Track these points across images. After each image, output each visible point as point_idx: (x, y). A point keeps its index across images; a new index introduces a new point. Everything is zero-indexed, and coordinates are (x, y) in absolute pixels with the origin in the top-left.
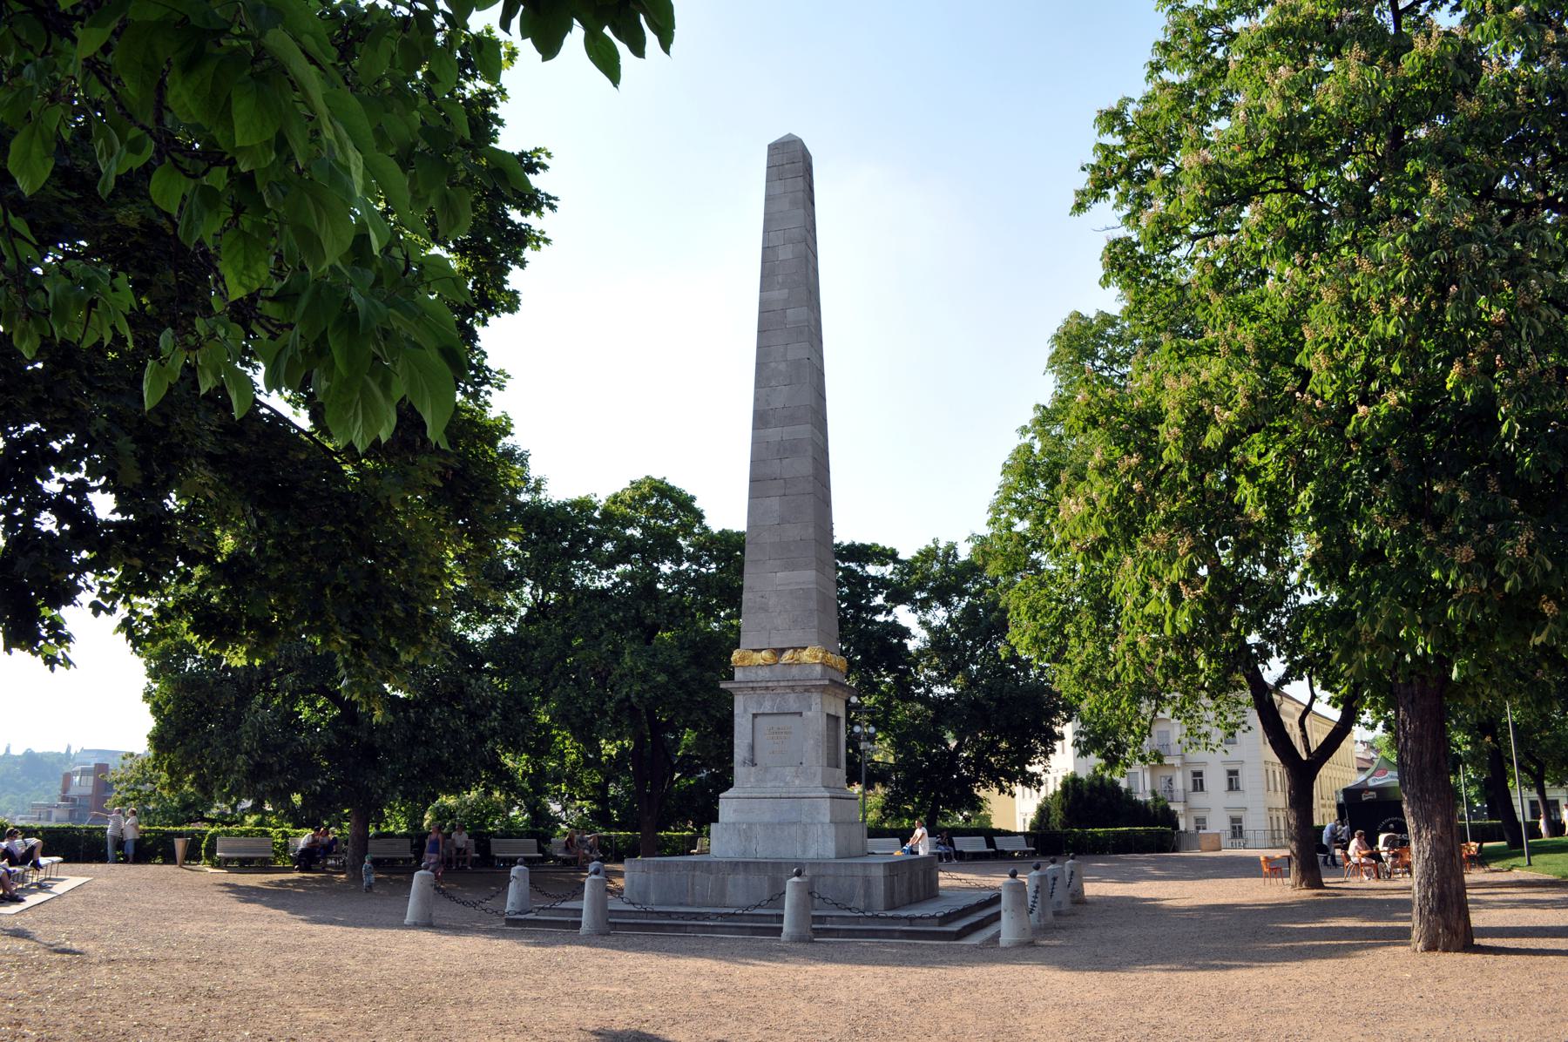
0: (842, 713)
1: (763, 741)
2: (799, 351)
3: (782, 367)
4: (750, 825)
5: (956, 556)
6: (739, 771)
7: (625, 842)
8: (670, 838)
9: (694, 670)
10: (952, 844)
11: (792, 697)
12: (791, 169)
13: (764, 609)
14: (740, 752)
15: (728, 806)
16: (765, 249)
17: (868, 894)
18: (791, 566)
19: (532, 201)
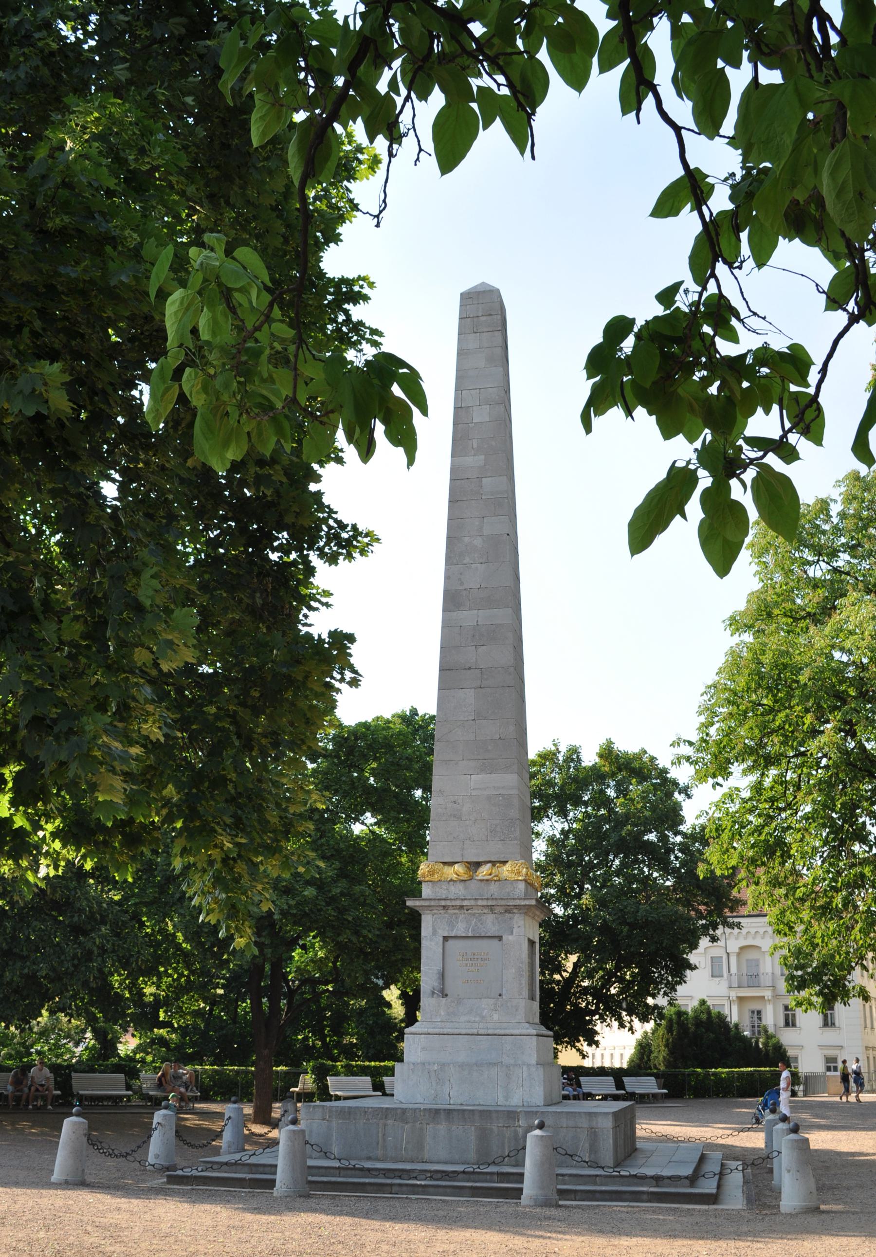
3: (478, 542)
4: (443, 1065)
5: (579, 760)
7: (211, 1077)
8: (212, 1065)
9: (343, 884)
10: (579, 1085)
11: (490, 918)
12: (639, 122)
13: (457, 816)
17: (594, 1148)
18: (488, 768)
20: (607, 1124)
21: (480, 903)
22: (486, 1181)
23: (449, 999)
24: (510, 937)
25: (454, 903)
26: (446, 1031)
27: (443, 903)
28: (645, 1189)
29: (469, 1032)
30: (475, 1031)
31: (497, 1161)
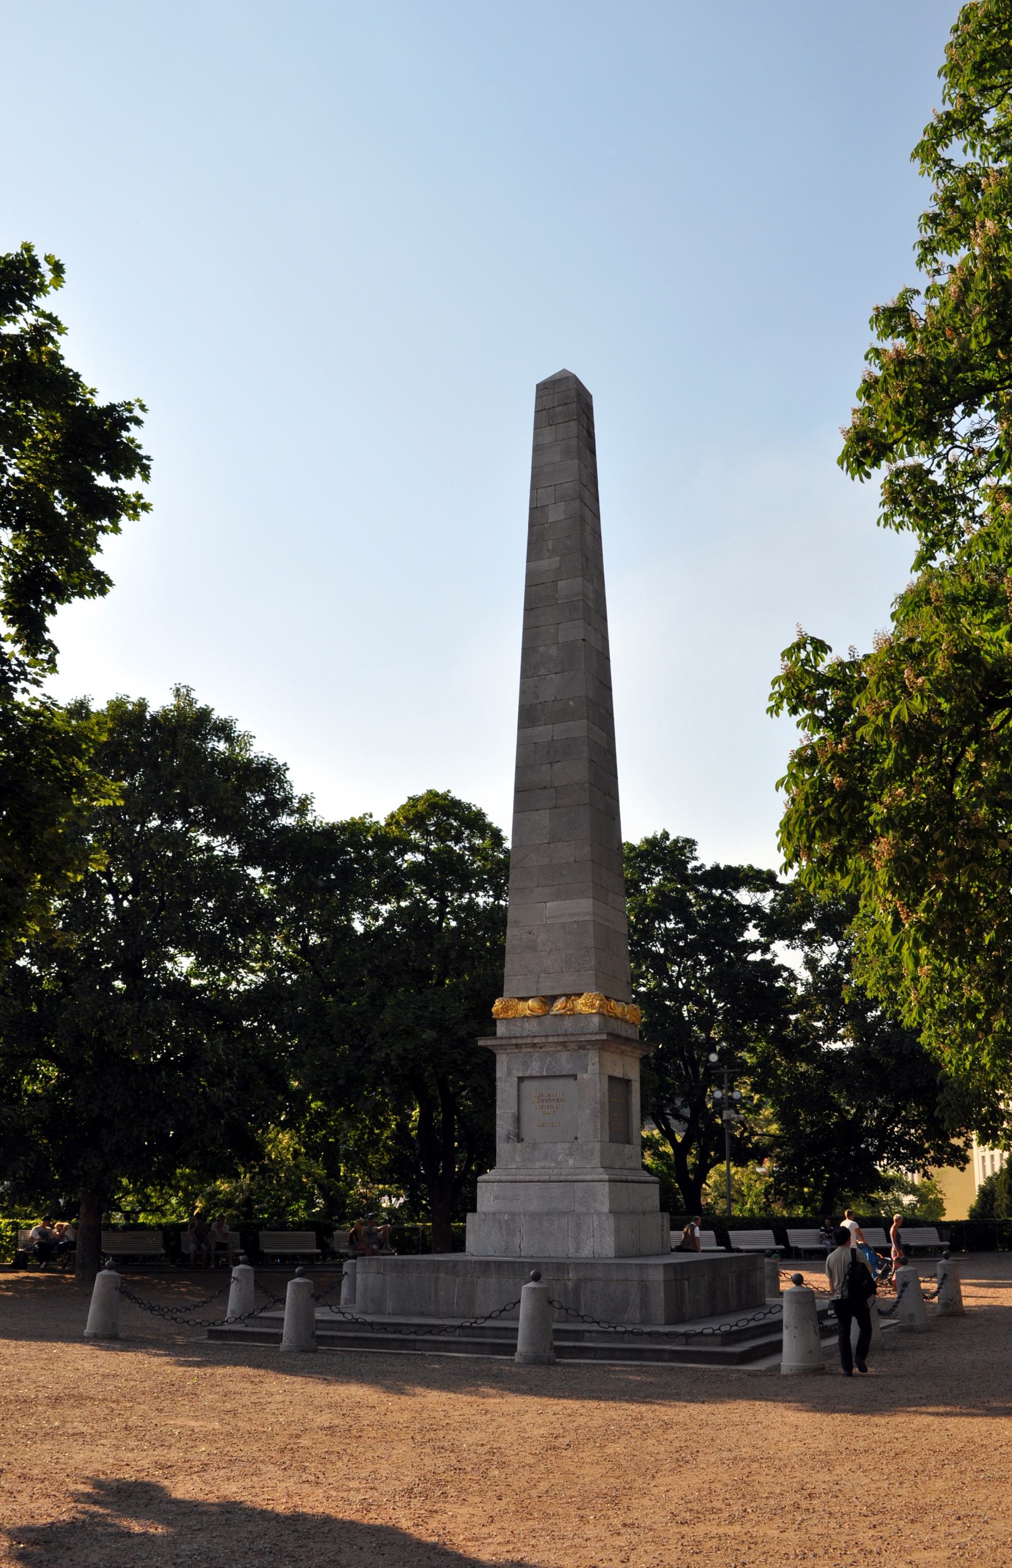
0: (634, 1074)
1: (531, 1112)
2: (574, 631)
3: (553, 651)
4: (513, 1215)
6: (502, 1148)
11: (564, 1056)
12: (565, 413)
13: (533, 948)
14: (503, 1125)
15: (489, 1193)
16: (533, 510)
19: (129, 461)
20: (657, 1276)
21: (551, 1039)
22: (326, 1330)
23: (525, 1144)
24: (585, 1076)
25: (524, 1041)
26: (518, 1178)
27: (514, 1041)
28: (667, 1347)
29: (541, 1178)
30: (547, 1178)
31: (493, 1315)
